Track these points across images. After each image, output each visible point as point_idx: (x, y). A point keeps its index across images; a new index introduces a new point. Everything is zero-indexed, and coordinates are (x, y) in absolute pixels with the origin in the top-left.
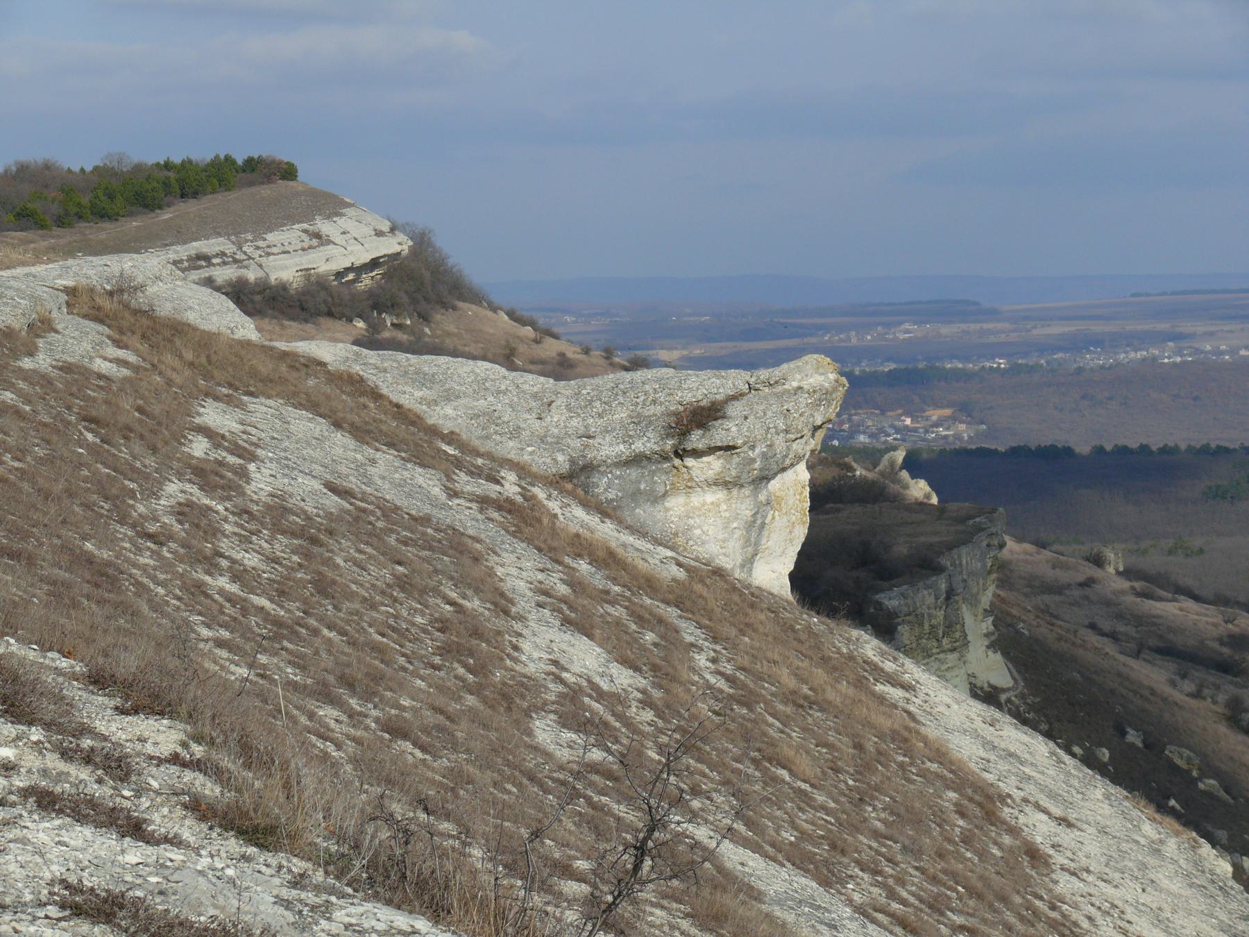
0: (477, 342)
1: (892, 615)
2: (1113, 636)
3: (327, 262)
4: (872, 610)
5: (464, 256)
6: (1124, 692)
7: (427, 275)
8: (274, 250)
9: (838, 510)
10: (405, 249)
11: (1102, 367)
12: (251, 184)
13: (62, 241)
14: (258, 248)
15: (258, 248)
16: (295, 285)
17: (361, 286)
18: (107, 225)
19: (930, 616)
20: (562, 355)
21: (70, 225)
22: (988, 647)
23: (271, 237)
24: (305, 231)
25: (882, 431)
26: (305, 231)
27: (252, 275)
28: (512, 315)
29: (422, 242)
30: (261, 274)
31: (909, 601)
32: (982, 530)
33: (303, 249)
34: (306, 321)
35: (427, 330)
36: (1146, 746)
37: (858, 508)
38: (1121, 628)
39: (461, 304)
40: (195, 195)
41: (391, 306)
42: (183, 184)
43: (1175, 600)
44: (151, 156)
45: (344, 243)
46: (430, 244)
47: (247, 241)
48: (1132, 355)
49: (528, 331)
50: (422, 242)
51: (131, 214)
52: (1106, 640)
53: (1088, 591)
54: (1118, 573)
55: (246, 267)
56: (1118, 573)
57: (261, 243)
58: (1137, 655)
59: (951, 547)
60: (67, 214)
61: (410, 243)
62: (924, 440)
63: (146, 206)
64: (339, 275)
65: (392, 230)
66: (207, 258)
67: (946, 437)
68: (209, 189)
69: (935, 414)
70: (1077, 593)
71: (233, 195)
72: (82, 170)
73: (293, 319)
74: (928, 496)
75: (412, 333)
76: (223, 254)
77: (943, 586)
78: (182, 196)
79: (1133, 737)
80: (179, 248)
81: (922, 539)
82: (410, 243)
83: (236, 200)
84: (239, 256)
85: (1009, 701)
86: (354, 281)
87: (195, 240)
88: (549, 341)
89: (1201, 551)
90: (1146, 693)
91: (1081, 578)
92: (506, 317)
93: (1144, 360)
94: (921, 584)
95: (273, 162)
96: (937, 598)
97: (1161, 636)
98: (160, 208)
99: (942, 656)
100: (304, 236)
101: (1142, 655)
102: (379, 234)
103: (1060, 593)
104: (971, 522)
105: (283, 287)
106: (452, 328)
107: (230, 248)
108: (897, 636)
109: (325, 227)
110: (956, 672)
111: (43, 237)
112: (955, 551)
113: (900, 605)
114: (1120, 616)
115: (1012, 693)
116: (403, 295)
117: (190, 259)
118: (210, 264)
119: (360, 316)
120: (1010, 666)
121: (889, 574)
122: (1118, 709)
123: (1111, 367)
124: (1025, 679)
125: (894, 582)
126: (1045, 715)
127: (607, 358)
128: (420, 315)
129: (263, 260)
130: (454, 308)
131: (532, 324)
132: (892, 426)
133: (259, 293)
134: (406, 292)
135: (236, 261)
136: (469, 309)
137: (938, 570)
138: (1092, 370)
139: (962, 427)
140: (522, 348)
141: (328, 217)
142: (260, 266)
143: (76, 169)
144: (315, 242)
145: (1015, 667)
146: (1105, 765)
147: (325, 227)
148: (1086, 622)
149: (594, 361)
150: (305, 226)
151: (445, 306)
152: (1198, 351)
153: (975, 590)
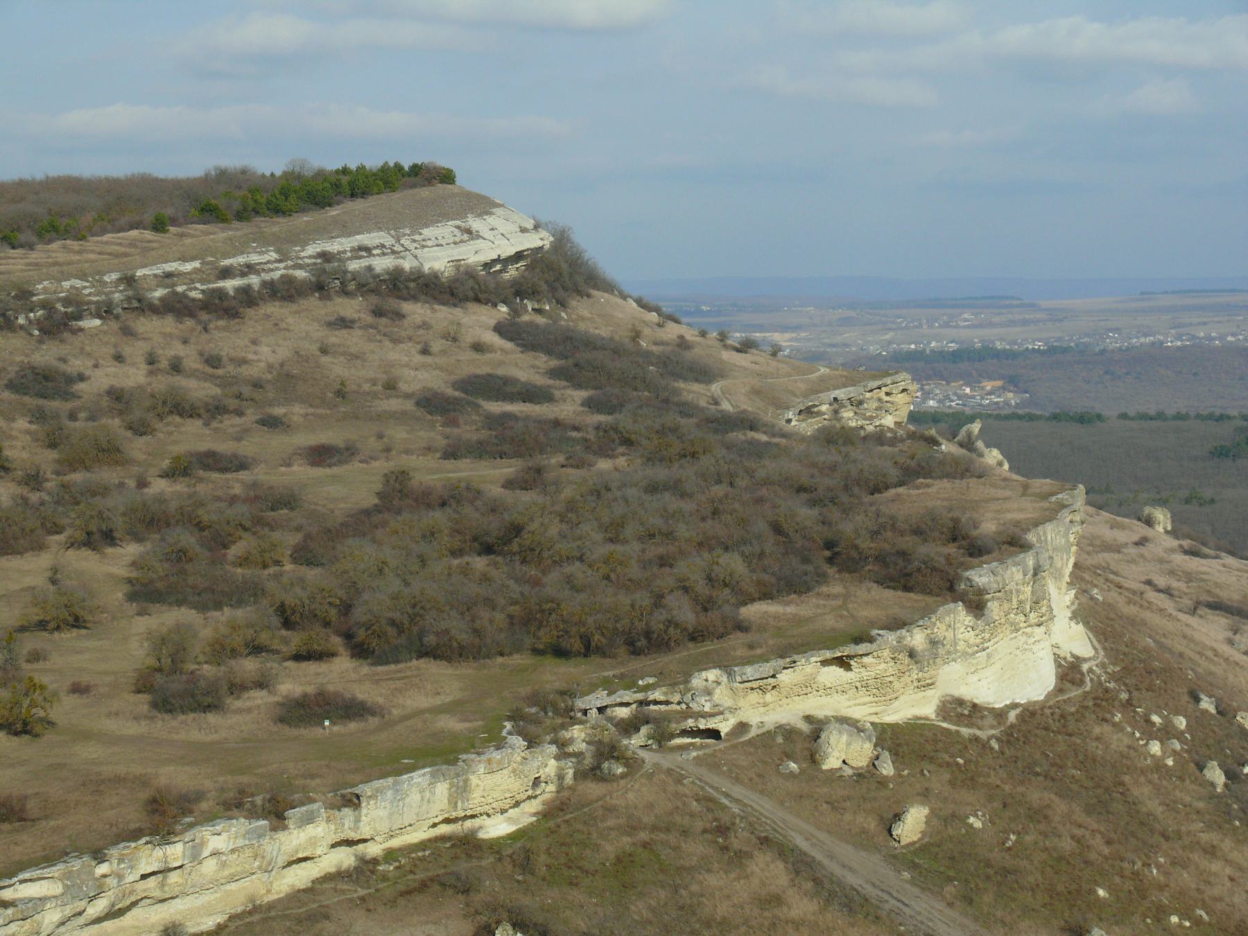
0: (607, 326)
1: (981, 592)
2: (1167, 591)
3: (476, 254)
4: (963, 587)
5: (596, 249)
6: (1192, 654)
7: (565, 266)
8: (429, 243)
9: (928, 486)
10: (547, 244)
11: (1120, 349)
12: (413, 186)
13: (239, 233)
14: (414, 241)
15: (414, 241)
16: (446, 274)
17: (506, 276)
18: (281, 220)
19: (1018, 591)
20: (681, 337)
21: (248, 219)
22: (1071, 619)
23: (426, 232)
24: (458, 227)
25: (947, 397)
26: (458, 227)
27: (407, 265)
28: (640, 302)
29: (561, 239)
30: (415, 264)
31: (999, 578)
32: (1065, 506)
33: (455, 243)
34: (455, 305)
35: (563, 314)
36: (1219, 712)
37: (945, 484)
38: (1175, 584)
39: (594, 292)
40: (364, 194)
41: (533, 294)
42: (352, 185)
43: (1217, 557)
44: (332, 164)
45: (492, 238)
46: (569, 240)
47: (405, 235)
48: (1142, 340)
49: (653, 317)
50: (561, 239)
51: (303, 211)
52: (1162, 596)
53: (1142, 550)
54: (1167, 532)
55: (403, 258)
56: (1167, 532)
57: (417, 237)
58: (1193, 611)
59: (1036, 525)
60: (245, 210)
61: (552, 239)
62: (980, 405)
63: (317, 204)
64: (487, 265)
65: (536, 227)
66: (368, 250)
67: (997, 403)
68: (376, 190)
69: (989, 386)
70: (1133, 551)
71: (396, 196)
72: (272, 174)
73: (443, 304)
74: (1000, 464)
75: (550, 317)
76: (383, 246)
77: (1031, 563)
78: (353, 195)
79: (1207, 704)
80: (343, 240)
81: (1009, 516)
82: (552, 239)
83: (397, 200)
84: (398, 248)
85: (1090, 670)
86: (500, 271)
87: (359, 233)
88: (671, 325)
89: (1212, 501)
90: (1210, 654)
91: (1136, 538)
92: (634, 305)
93: (1153, 343)
94: (1009, 561)
95: (435, 168)
96: (1025, 575)
97: (1208, 591)
98: (330, 205)
99: (1029, 630)
100: (457, 232)
101: (1199, 612)
102: (524, 230)
103: (1119, 552)
104: (1053, 499)
105: (435, 275)
106: (586, 313)
107: (388, 240)
108: (986, 612)
109: (475, 224)
110: (1042, 644)
111: (223, 230)
112: (1040, 528)
113: (990, 582)
114: (1172, 573)
115: (1093, 663)
116: (542, 283)
117: (353, 249)
118: (370, 255)
119: (504, 302)
120: (1091, 636)
121: (977, 551)
122: (1191, 675)
123: (1128, 349)
124: (1105, 649)
125: (985, 558)
126: (1126, 685)
127: (721, 340)
128: (558, 302)
129: (418, 252)
130: (589, 296)
131: (657, 310)
132: (955, 394)
133: (414, 280)
134: (546, 282)
135: (394, 252)
136: (601, 296)
137: (1025, 547)
138: (1113, 351)
139: (1011, 395)
140: (646, 331)
141: (480, 215)
142: (416, 257)
143: (268, 174)
144: (466, 237)
145: (1096, 637)
146: (1182, 732)
147: (475, 224)
148: (1143, 579)
149: (710, 343)
150: (458, 223)
151: (581, 294)
152: (1194, 337)
153: (1059, 565)
